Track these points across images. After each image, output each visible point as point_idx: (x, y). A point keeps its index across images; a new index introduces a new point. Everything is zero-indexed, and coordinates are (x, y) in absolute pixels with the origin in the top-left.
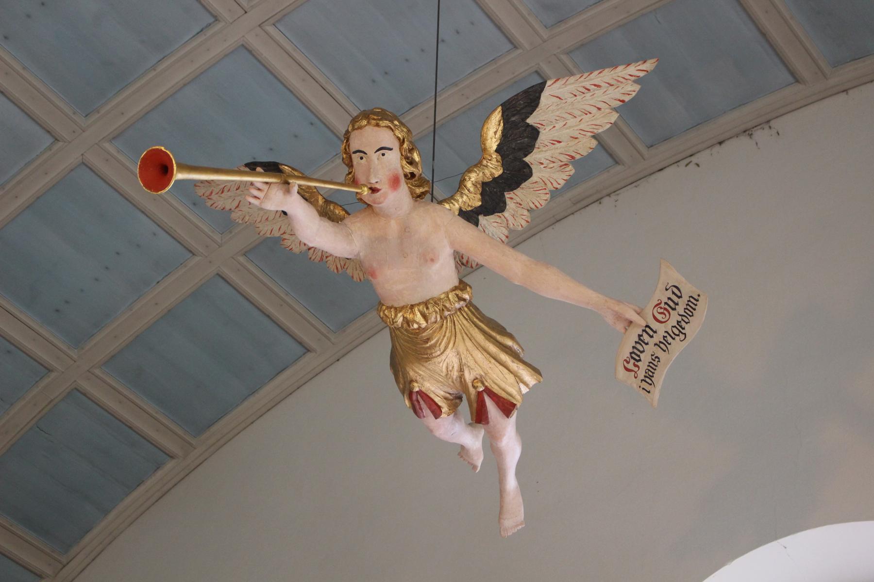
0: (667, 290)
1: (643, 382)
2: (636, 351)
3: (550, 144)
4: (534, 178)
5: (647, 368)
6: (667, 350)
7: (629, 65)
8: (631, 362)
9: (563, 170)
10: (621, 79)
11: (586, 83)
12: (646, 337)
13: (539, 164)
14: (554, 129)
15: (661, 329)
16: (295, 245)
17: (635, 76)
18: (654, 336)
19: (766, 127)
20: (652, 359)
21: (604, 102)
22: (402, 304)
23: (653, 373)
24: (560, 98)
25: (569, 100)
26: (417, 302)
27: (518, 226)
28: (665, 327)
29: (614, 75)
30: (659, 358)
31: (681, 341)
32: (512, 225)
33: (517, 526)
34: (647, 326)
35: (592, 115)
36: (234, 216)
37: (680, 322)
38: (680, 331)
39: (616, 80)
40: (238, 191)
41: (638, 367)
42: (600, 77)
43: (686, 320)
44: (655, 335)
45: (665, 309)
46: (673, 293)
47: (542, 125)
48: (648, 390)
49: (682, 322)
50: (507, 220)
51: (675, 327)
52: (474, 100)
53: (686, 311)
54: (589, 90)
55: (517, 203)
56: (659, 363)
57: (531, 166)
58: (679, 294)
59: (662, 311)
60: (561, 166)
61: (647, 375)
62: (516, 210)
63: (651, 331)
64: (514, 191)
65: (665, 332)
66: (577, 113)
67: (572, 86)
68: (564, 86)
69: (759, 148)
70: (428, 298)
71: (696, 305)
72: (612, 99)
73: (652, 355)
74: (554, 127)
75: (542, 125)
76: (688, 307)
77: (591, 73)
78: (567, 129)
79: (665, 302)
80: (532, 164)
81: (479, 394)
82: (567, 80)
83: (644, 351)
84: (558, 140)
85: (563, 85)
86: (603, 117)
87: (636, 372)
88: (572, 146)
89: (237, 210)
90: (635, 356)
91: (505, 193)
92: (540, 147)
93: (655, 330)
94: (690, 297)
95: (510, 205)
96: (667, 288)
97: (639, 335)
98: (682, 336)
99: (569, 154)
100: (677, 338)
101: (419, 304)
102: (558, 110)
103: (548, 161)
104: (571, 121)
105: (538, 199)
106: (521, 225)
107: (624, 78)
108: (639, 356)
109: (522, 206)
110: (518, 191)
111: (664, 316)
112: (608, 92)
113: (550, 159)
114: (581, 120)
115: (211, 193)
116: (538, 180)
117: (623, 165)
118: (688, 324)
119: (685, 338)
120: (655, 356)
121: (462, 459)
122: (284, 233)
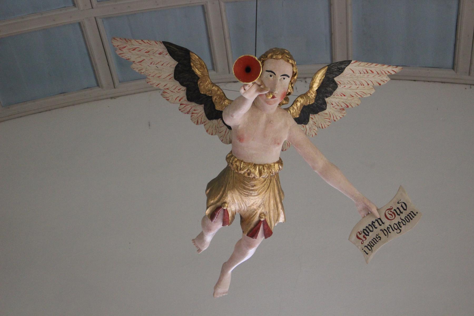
0: (398, 203)
1: (366, 247)
2: (367, 229)
3: (340, 95)
4: (326, 111)
5: (371, 241)
6: (387, 235)
7: (390, 66)
8: (362, 234)
9: (341, 112)
10: (383, 72)
11: (367, 68)
12: (376, 224)
13: (331, 104)
14: (345, 87)
15: (387, 223)
16: (172, 98)
17: (390, 73)
18: (382, 225)
19: (304, 81)
20: (376, 237)
21: (372, 82)
22: (249, 161)
23: (374, 245)
24: (353, 72)
25: (357, 75)
26: (259, 163)
27: (311, 135)
28: (390, 222)
29: (382, 69)
30: (380, 238)
31: (397, 233)
32: (308, 133)
33: (224, 293)
34: (380, 219)
35: (364, 86)
36: (134, 66)
37: (400, 223)
38: (398, 228)
39: (381, 71)
40: (146, 53)
41: (366, 238)
42: (375, 68)
43: (404, 223)
44: (382, 225)
45: (393, 213)
46: (402, 206)
47: (340, 83)
48: (367, 253)
49: (401, 223)
50: (306, 130)
51: (396, 224)
52: (161, 8)
53: (406, 218)
54: (368, 72)
55: (314, 122)
56: (379, 240)
57: (327, 104)
58: (405, 208)
59: (391, 213)
60: (340, 109)
61: (370, 244)
62: (312, 126)
63: (381, 222)
64: (315, 115)
65: (389, 225)
66: (358, 83)
67: (361, 68)
68: (358, 66)
69: (297, 92)
70: (265, 163)
71: (413, 217)
72: (376, 81)
73: (377, 235)
74: (345, 86)
75: (340, 83)
76: (408, 217)
77: (372, 64)
78: (350, 89)
79: (415, 216)
80: (328, 103)
81: (259, 222)
82: (360, 63)
83: (372, 231)
84: (344, 94)
85: (358, 65)
86: (368, 89)
87: (363, 241)
88: (349, 100)
89: (138, 64)
90: (366, 232)
91: (310, 114)
92: (335, 95)
93: (383, 222)
94: (411, 212)
95: (311, 121)
96: (399, 202)
97: (372, 221)
98: (399, 231)
99: (346, 104)
100: (395, 230)
101: (260, 165)
102: (350, 78)
103: (336, 104)
104: (354, 87)
105: (324, 123)
106: (312, 135)
107: (385, 72)
108: (368, 233)
109: (315, 125)
110: (316, 116)
111: (391, 216)
112: (375, 77)
113: (337, 104)
114: (358, 87)
115: (125, 47)
116: (328, 113)
117: (217, 72)
118: (405, 225)
119: (399, 233)
120: (379, 236)
121: (194, 243)
122: (168, 89)
